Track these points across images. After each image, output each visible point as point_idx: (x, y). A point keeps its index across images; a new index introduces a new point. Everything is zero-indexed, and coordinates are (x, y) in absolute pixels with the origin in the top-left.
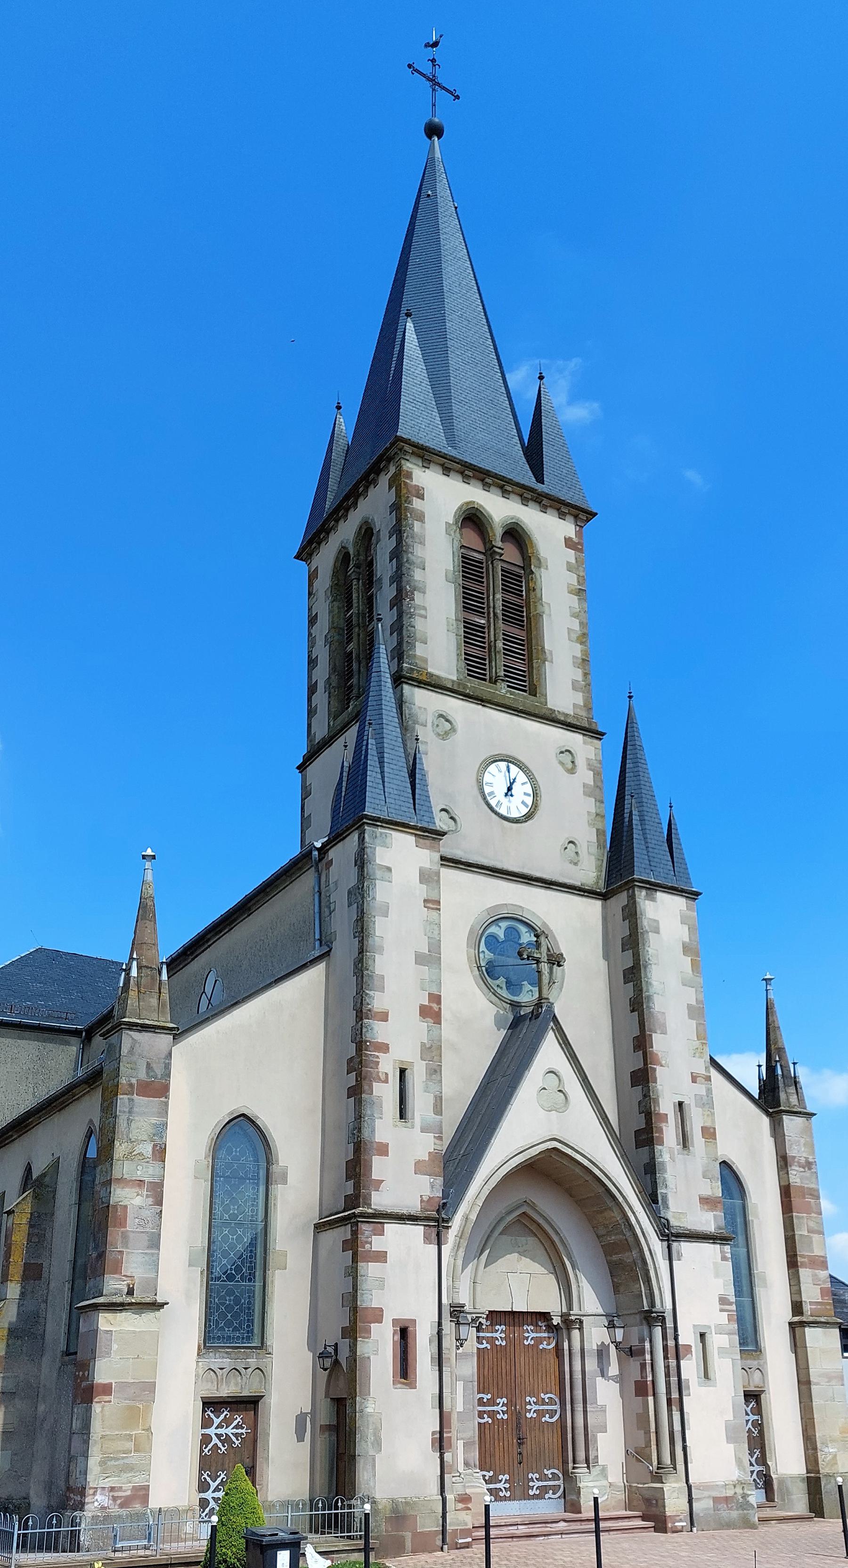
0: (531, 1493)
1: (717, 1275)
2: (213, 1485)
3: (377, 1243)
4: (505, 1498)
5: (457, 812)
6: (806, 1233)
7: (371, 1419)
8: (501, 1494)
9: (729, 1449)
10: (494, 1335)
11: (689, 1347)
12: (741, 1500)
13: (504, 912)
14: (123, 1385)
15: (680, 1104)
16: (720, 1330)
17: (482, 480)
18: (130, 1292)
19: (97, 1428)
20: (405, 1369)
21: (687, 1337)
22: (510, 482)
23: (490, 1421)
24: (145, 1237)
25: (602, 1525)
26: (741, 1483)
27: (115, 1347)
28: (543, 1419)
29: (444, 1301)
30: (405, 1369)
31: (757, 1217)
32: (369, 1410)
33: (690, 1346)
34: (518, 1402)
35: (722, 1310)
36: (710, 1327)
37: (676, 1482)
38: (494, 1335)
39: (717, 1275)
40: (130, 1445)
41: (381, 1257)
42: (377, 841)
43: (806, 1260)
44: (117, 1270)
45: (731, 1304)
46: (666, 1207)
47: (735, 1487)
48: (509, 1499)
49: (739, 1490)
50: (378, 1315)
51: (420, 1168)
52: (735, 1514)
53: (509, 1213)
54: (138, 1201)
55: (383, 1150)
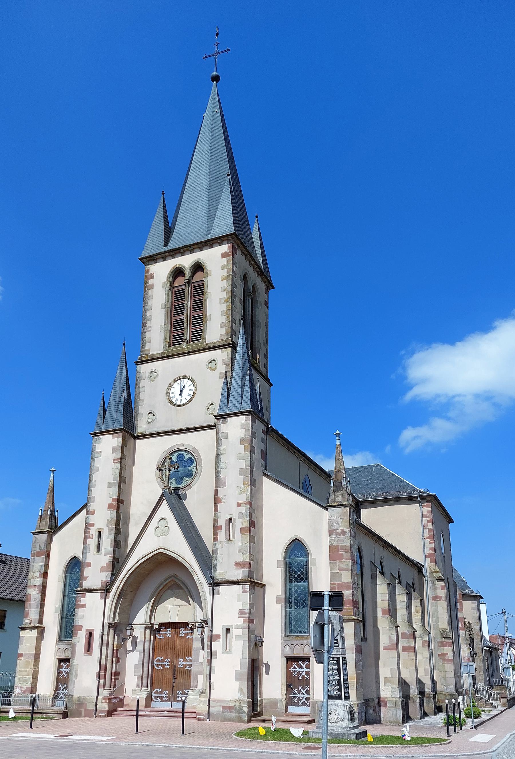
0: (177, 699)
1: (239, 600)
2: (304, 700)
3: (82, 601)
4: (165, 701)
5: (155, 412)
6: (338, 571)
7: (75, 667)
8: (164, 699)
9: (236, 685)
10: (167, 633)
11: (218, 636)
12: (238, 708)
13: (175, 449)
14: (26, 654)
15: (231, 519)
16: (238, 627)
17: (179, 252)
18: (30, 623)
19: (18, 668)
20: (89, 648)
21: (218, 630)
22: (190, 246)
23: (162, 668)
24: (36, 604)
25: (186, 715)
26: (240, 701)
27: (24, 641)
28: (186, 668)
29: (106, 621)
30: (89, 648)
31: (315, 565)
32: (74, 663)
33: (219, 635)
34: (175, 661)
35: (239, 617)
36: (232, 626)
37: (205, 697)
38: (167, 633)
39: (239, 600)
40: (26, 673)
41: (84, 606)
42: (97, 442)
43: (336, 586)
44: (27, 616)
45: (246, 614)
46: (216, 570)
47: (235, 702)
48: (167, 701)
49: (238, 704)
50: (80, 628)
51: (102, 570)
52: (234, 715)
53: (165, 581)
54: (34, 593)
55: (89, 565)
